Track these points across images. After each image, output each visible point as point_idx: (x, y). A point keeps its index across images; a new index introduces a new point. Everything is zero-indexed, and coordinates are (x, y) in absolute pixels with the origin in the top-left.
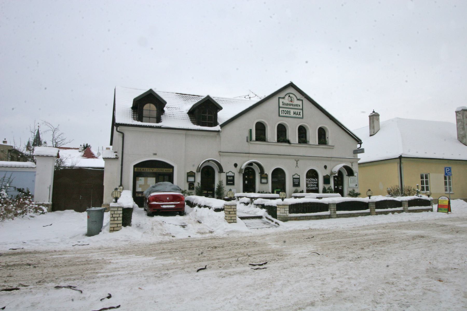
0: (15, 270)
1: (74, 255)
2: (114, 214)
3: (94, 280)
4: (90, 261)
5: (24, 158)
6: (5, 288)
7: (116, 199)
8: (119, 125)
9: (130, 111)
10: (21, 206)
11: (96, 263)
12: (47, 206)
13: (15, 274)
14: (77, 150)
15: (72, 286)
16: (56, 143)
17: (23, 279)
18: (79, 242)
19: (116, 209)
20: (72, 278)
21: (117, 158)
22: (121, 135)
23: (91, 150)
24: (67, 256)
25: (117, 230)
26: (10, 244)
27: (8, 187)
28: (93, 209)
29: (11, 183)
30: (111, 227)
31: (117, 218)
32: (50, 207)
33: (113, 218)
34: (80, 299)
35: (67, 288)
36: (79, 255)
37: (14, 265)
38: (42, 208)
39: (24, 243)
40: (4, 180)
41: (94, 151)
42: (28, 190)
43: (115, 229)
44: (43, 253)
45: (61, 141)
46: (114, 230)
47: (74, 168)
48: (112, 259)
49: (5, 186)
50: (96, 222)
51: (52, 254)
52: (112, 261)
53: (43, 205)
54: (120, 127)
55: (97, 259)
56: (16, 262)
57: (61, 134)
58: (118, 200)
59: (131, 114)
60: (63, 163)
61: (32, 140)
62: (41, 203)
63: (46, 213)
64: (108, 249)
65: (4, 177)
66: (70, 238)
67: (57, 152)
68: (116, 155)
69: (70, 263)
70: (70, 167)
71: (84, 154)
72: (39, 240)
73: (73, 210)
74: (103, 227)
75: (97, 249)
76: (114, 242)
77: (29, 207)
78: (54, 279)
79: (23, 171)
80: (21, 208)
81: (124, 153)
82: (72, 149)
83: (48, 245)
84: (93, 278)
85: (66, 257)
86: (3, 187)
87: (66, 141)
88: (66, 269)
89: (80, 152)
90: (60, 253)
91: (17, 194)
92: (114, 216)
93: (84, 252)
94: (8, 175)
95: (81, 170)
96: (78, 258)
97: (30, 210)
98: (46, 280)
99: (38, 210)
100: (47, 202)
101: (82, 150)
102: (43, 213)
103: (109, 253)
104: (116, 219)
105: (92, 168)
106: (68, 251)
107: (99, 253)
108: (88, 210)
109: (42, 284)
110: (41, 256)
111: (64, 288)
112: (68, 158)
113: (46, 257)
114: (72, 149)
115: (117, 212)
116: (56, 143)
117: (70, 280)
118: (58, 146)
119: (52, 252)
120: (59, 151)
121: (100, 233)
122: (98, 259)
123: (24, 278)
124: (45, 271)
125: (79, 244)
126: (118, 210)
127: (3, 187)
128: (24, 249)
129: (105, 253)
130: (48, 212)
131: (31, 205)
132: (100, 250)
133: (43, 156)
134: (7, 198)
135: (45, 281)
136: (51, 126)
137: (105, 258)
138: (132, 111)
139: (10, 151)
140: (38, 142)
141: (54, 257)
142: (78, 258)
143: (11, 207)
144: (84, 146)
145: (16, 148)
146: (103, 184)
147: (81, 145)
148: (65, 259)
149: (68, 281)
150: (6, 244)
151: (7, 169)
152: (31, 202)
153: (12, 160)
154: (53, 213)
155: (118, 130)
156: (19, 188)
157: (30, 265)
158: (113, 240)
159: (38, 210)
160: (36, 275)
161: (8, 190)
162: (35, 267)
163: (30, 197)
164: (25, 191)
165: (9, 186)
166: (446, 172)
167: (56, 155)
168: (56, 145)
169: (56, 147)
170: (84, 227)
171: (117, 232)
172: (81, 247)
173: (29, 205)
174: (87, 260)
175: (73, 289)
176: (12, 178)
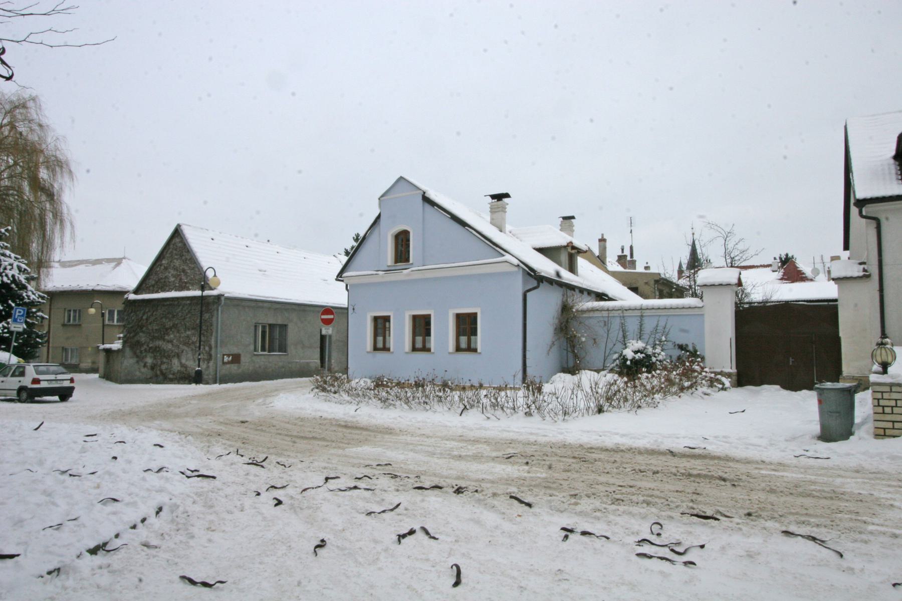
0: (702, 484)
1: (802, 476)
2: (882, 399)
3: (864, 537)
4: (842, 494)
5: (680, 292)
6: (695, 512)
7: (885, 366)
8: (862, 203)
9: (889, 165)
10: (688, 373)
11: (857, 501)
12: (728, 375)
13: (703, 491)
14: (768, 269)
15: (818, 538)
16: (732, 259)
17: (720, 504)
18: (807, 451)
19: (887, 389)
20: (813, 522)
21: (867, 276)
22: (873, 224)
23: (798, 266)
24: (789, 475)
25: (895, 434)
26: (684, 438)
27: (664, 341)
28: (829, 385)
29: (667, 335)
30: (876, 428)
31: (890, 408)
32: (735, 378)
33: (881, 408)
34: (843, 569)
35: (807, 538)
36: (813, 478)
37: (699, 475)
38: (720, 380)
39: (706, 439)
40: (658, 331)
41: (804, 266)
42: (694, 348)
43: (888, 432)
44: (742, 463)
45: (741, 255)
46: (885, 436)
47: (769, 304)
48: (895, 500)
49: (660, 341)
50: (838, 412)
51: (758, 466)
52: (896, 504)
53: (721, 373)
54: (867, 205)
55: (857, 491)
56: (700, 470)
57: (739, 242)
58: (890, 369)
59: (894, 171)
60: (747, 295)
61: (685, 260)
62: (718, 370)
63: (728, 389)
64: (877, 475)
65: (657, 326)
66: (787, 441)
67: (737, 276)
68: (864, 270)
69: (800, 490)
70: (761, 303)
71: (783, 275)
72: (729, 437)
73: (778, 387)
74: (854, 427)
75: (852, 471)
76: (888, 461)
77: (700, 376)
78: (776, 515)
79: (680, 315)
80: (688, 379)
81: (884, 263)
82: (757, 267)
83: (747, 448)
84: (860, 533)
85: (787, 477)
86: (657, 343)
87: (751, 252)
88: (792, 500)
89: (773, 271)
90: (773, 467)
91: (678, 355)
92: (882, 403)
93: (822, 472)
94: (662, 324)
95: (786, 307)
96: (814, 483)
97: (702, 383)
98: (761, 513)
99: (715, 384)
100: (727, 370)
101: (779, 268)
102: (724, 389)
103: (882, 485)
104: (888, 410)
105: (804, 301)
106: (789, 466)
107: (858, 480)
108: (818, 388)
109: (755, 521)
110: (741, 467)
111: (800, 538)
112: (758, 285)
113: (749, 471)
114: (757, 267)
115: (890, 395)
116: (732, 259)
117: (809, 524)
118: (735, 264)
119: (757, 462)
120: (740, 274)
121: (851, 437)
122: (860, 494)
123: (721, 502)
124: (754, 496)
125: (808, 454)
126: (891, 391)
127: (657, 343)
128: (707, 450)
129: (873, 482)
130: (733, 387)
131: (704, 374)
132: (857, 475)
133: (714, 285)
134: (665, 360)
135: (761, 516)
136: (720, 230)
137: (876, 494)
138: (895, 164)
139: (657, 282)
140: (695, 262)
141: (763, 472)
142: (813, 483)
143: (673, 376)
144: (781, 258)
145: (667, 276)
146: (837, 332)
147: (775, 259)
148: (786, 479)
149: (804, 525)
150: (678, 438)
151: (672, 312)
152: (702, 368)
153: (661, 296)
154: (740, 390)
155: (864, 213)
156: (680, 343)
157: (724, 480)
158: (888, 458)
159: (715, 384)
160: (741, 501)
161: (665, 347)
162: (734, 485)
163: (699, 359)
164: (690, 348)
165: (665, 341)
166: (16, 317)
167: (735, 281)
168: (732, 264)
169: (732, 266)
170: (811, 421)
171: (892, 439)
172: (812, 462)
173: (701, 374)
174: (834, 492)
175: (820, 545)
176: (668, 326)
